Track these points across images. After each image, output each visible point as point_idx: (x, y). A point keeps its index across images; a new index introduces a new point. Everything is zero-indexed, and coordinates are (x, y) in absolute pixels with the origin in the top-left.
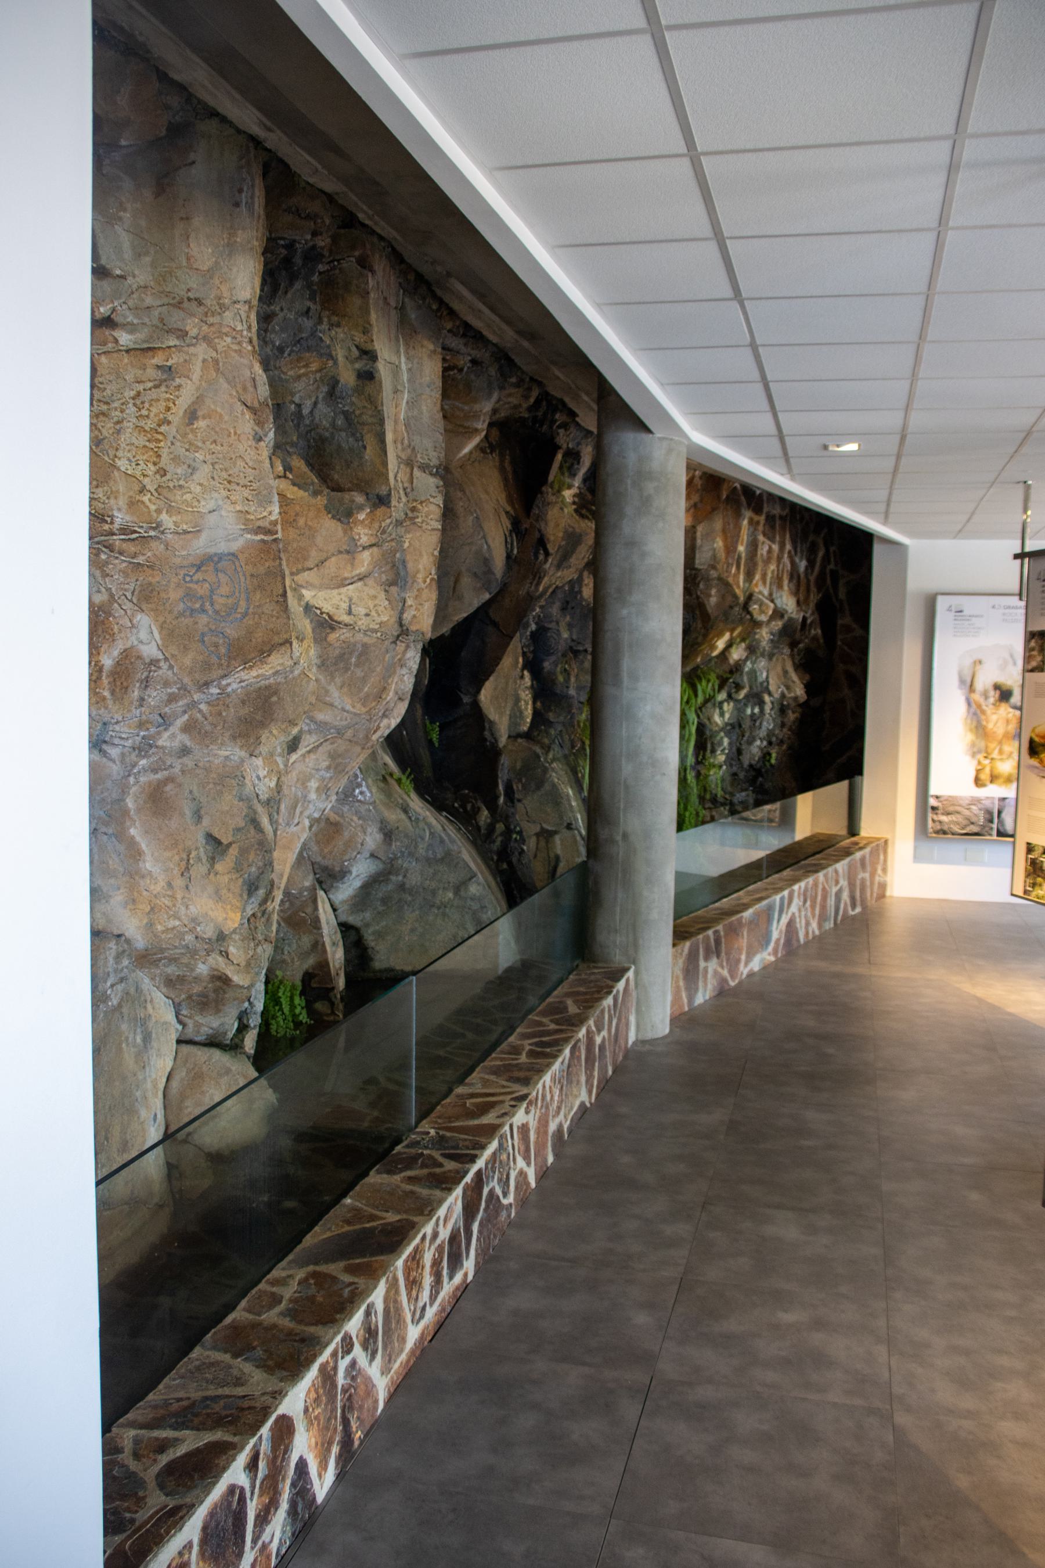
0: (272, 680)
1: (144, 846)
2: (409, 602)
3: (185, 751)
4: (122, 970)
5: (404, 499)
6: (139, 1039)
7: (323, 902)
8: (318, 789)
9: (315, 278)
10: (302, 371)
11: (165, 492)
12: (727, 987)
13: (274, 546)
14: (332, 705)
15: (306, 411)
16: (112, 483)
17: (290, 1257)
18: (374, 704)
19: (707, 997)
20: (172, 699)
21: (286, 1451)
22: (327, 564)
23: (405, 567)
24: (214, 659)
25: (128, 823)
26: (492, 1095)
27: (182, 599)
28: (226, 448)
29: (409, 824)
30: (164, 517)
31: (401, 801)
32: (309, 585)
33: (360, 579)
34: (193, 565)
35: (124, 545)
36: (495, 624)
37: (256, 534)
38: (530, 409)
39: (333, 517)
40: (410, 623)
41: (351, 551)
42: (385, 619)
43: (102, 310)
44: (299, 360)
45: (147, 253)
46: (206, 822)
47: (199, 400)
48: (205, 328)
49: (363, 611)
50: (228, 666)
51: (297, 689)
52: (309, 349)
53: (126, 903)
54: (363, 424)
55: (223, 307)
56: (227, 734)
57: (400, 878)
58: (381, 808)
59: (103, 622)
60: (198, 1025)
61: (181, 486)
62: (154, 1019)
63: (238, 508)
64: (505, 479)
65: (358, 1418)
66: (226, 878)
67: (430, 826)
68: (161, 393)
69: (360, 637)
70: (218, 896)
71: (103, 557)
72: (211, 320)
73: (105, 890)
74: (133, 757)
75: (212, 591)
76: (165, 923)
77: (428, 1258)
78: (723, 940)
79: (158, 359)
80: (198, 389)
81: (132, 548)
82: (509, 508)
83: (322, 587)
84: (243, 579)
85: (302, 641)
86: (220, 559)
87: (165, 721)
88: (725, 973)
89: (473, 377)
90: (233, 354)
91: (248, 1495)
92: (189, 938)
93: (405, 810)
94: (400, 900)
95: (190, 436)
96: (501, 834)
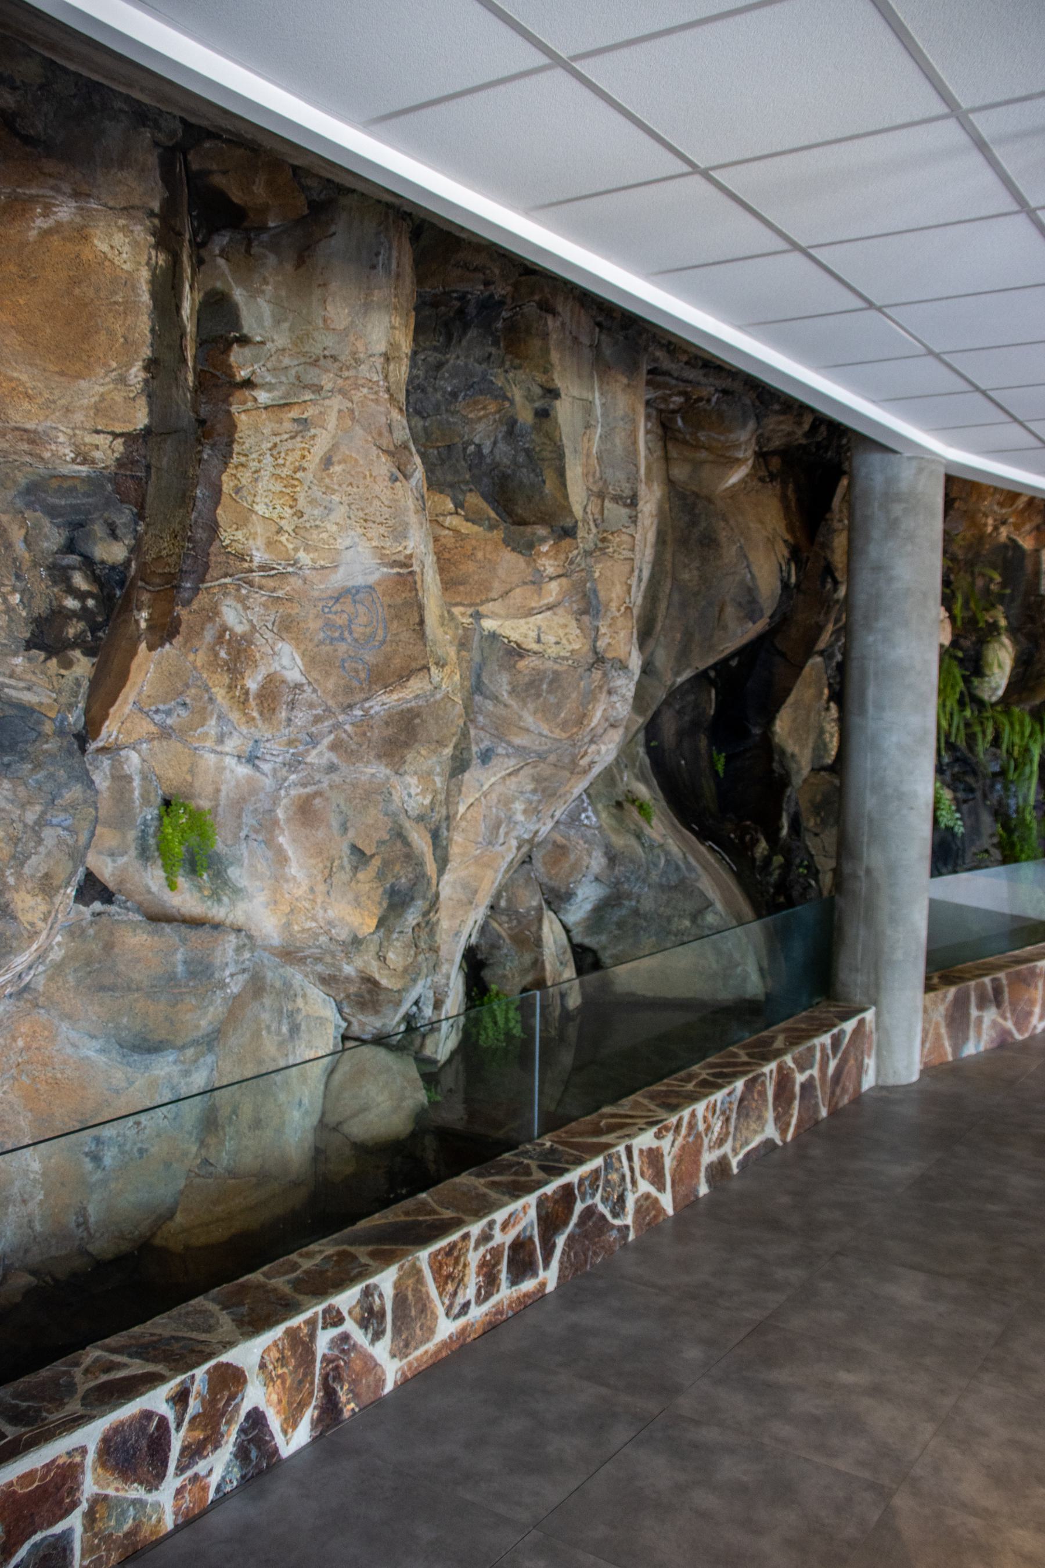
0: (413, 704)
1: (290, 853)
2: (603, 630)
3: (332, 768)
4: (243, 962)
5: (594, 530)
6: (285, 1029)
7: (551, 922)
8: (525, 812)
9: (500, 325)
10: (482, 413)
11: (302, 532)
12: (1010, 1040)
13: (410, 578)
14: (528, 730)
15: (486, 451)
16: (250, 526)
17: (335, 1236)
18: (575, 730)
19: (982, 1048)
20: (317, 720)
21: (232, 1397)
22: (511, 594)
23: (597, 597)
24: (355, 684)
25: (277, 832)
26: (631, 1117)
27: (321, 629)
28: (362, 490)
29: (640, 850)
30: (301, 554)
31: (632, 827)
32: (494, 615)
33: (549, 609)
34: (331, 598)
35: (264, 581)
36: (783, 655)
37: (392, 567)
38: (807, 435)
39: (513, 550)
40: (605, 651)
41: (537, 582)
42: (577, 646)
43: (243, 373)
44: (475, 403)
45: (285, 320)
46: (351, 833)
47: (335, 447)
48: (340, 381)
49: (552, 639)
50: (370, 690)
51: (441, 712)
52: (481, 392)
53: (268, 904)
54: (543, 460)
55: (358, 362)
56: (372, 753)
57: (633, 903)
58: (609, 832)
59: (245, 650)
60: (362, 1024)
61: (317, 526)
62: (304, 1013)
63: (374, 544)
64: (786, 508)
65: (350, 1391)
66: (367, 887)
67: (667, 853)
68: (298, 442)
69: (549, 664)
70: (357, 902)
71: (244, 592)
72: (346, 374)
73: (250, 890)
74: (284, 770)
75: (350, 621)
76: (303, 924)
77: (474, 1258)
78: (1006, 990)
79: (294, 413)
80: (334, 437)
81: (271, 583)
82: (787, 537)
83: (508, 617)
84: (380, 610)
85: (443, 666)
86: (358, 592)
87: (314, 740)
88: (1009, 1025)
89: (724, 407)
90: (370, 403)
91: (172, 1426)
92: (323, 939)
93: (639, 836)
94: (635, 925)
95: (327, 480)
96: (780, 867)
